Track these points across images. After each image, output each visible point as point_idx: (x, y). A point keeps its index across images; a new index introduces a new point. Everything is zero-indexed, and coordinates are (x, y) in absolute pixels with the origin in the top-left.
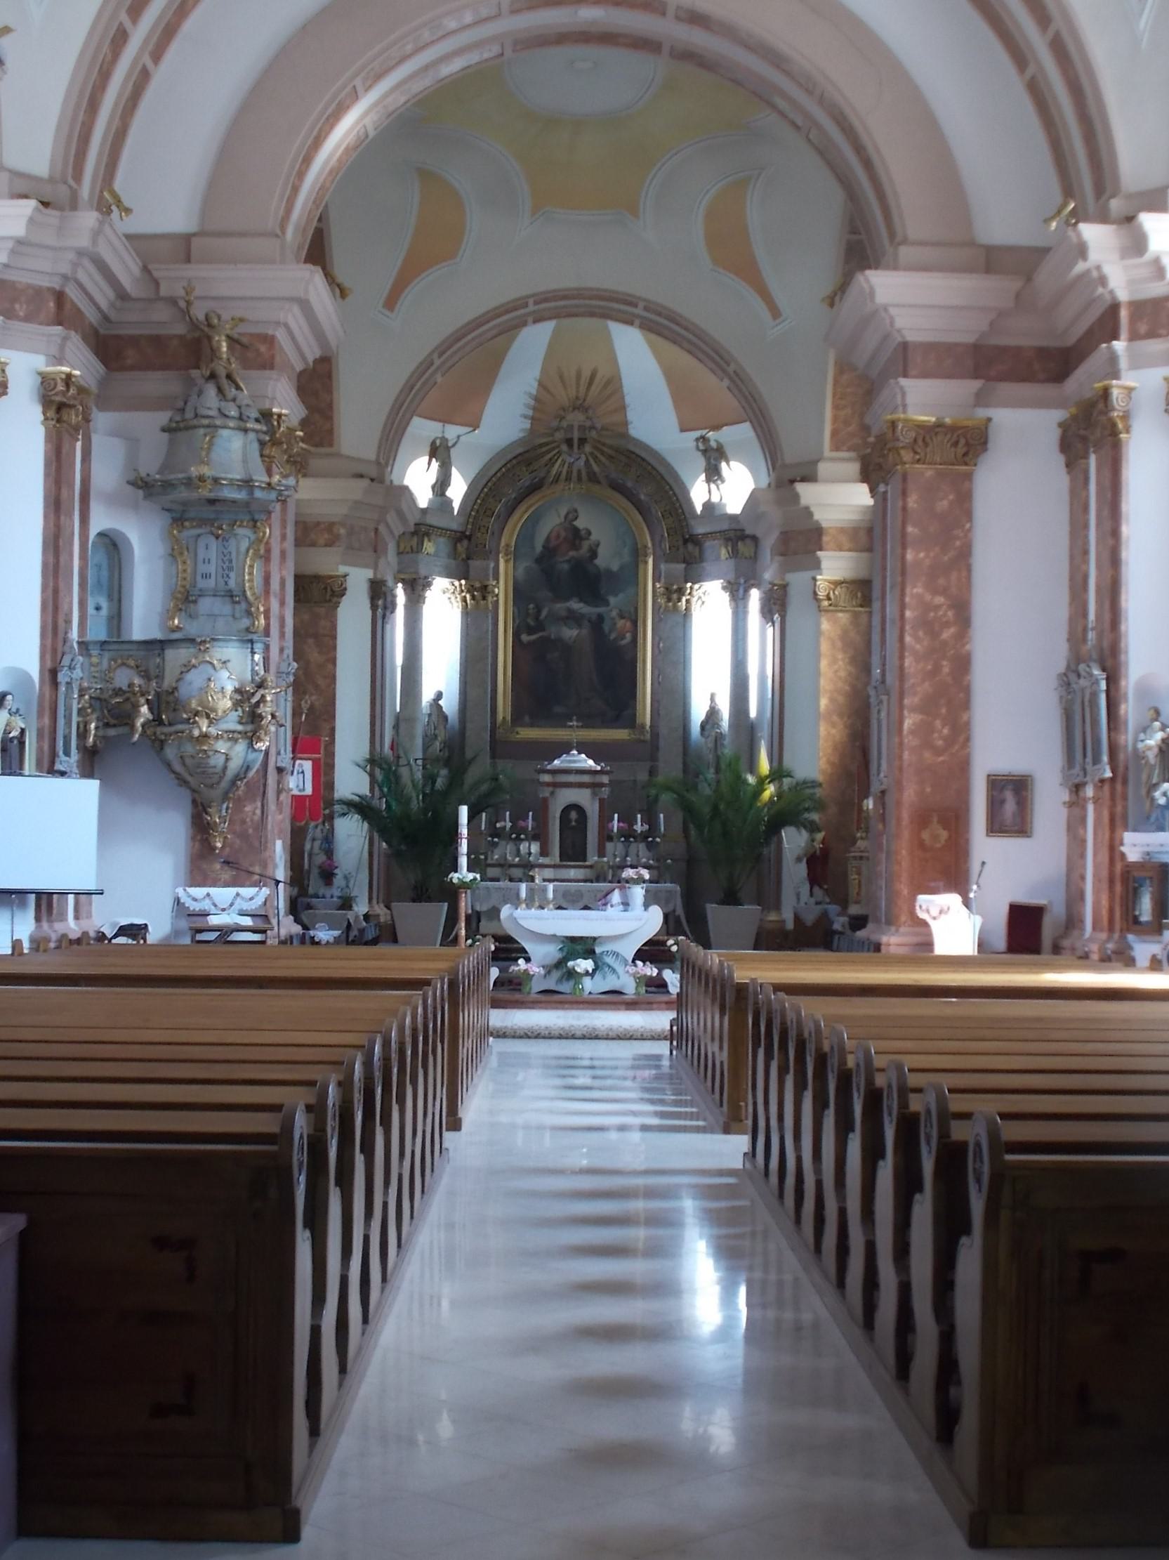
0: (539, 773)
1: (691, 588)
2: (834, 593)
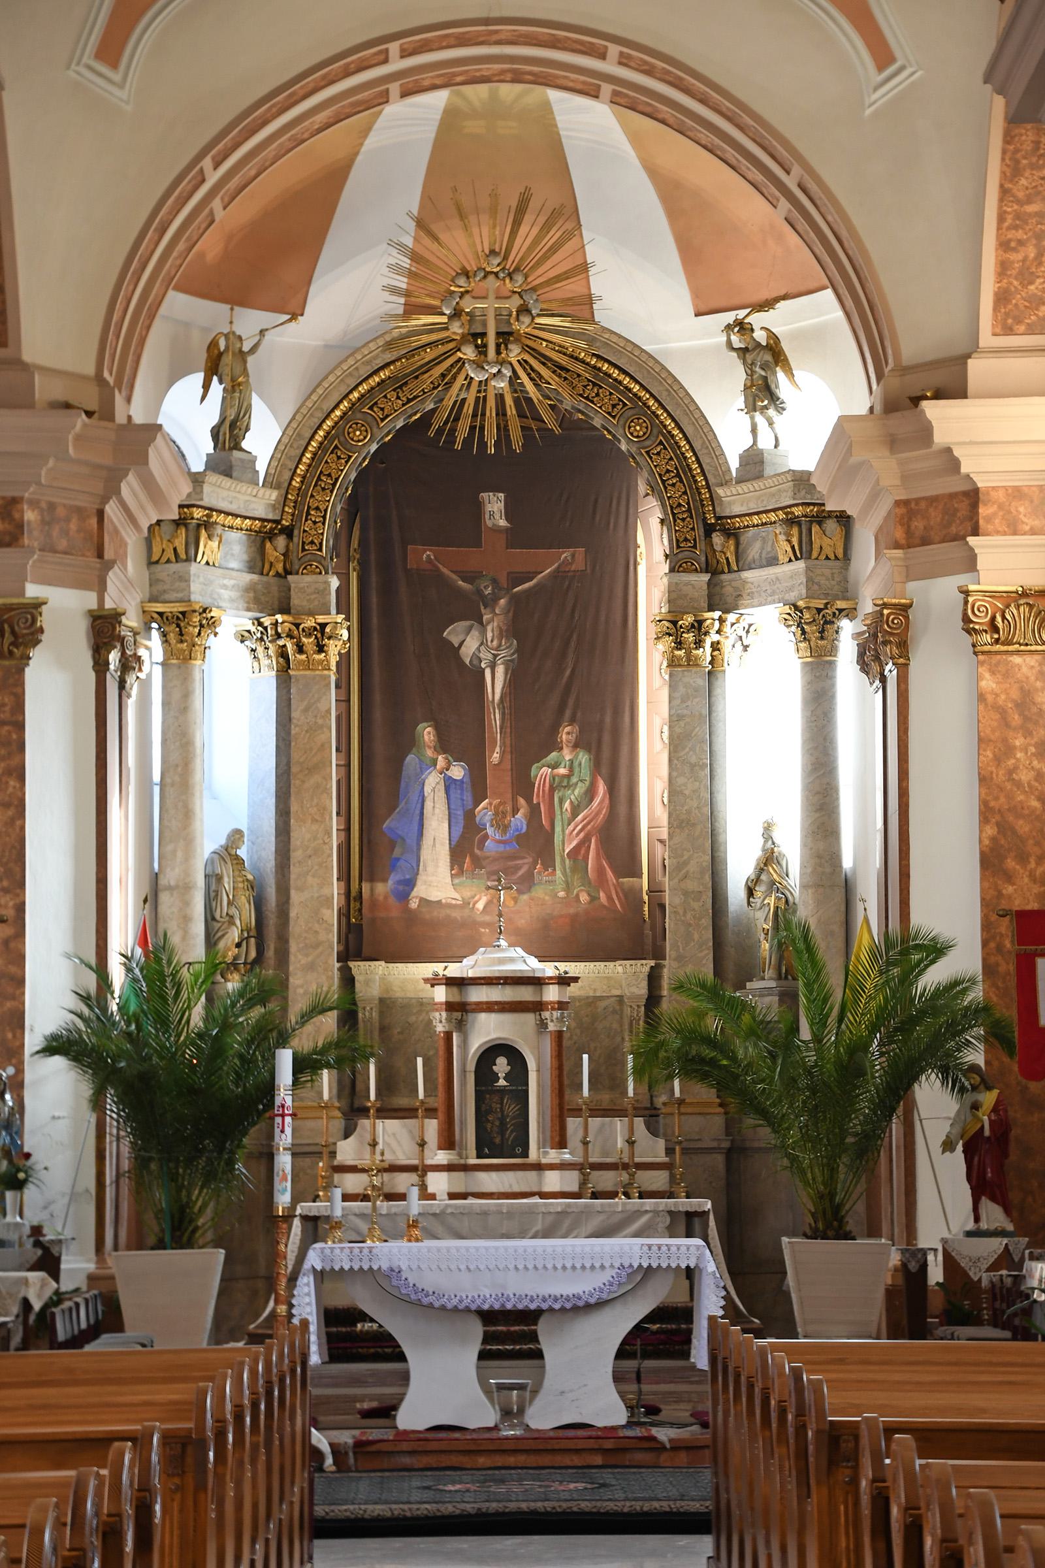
0: (433, 986)
1: (722, 620)
2: (1004, 618)
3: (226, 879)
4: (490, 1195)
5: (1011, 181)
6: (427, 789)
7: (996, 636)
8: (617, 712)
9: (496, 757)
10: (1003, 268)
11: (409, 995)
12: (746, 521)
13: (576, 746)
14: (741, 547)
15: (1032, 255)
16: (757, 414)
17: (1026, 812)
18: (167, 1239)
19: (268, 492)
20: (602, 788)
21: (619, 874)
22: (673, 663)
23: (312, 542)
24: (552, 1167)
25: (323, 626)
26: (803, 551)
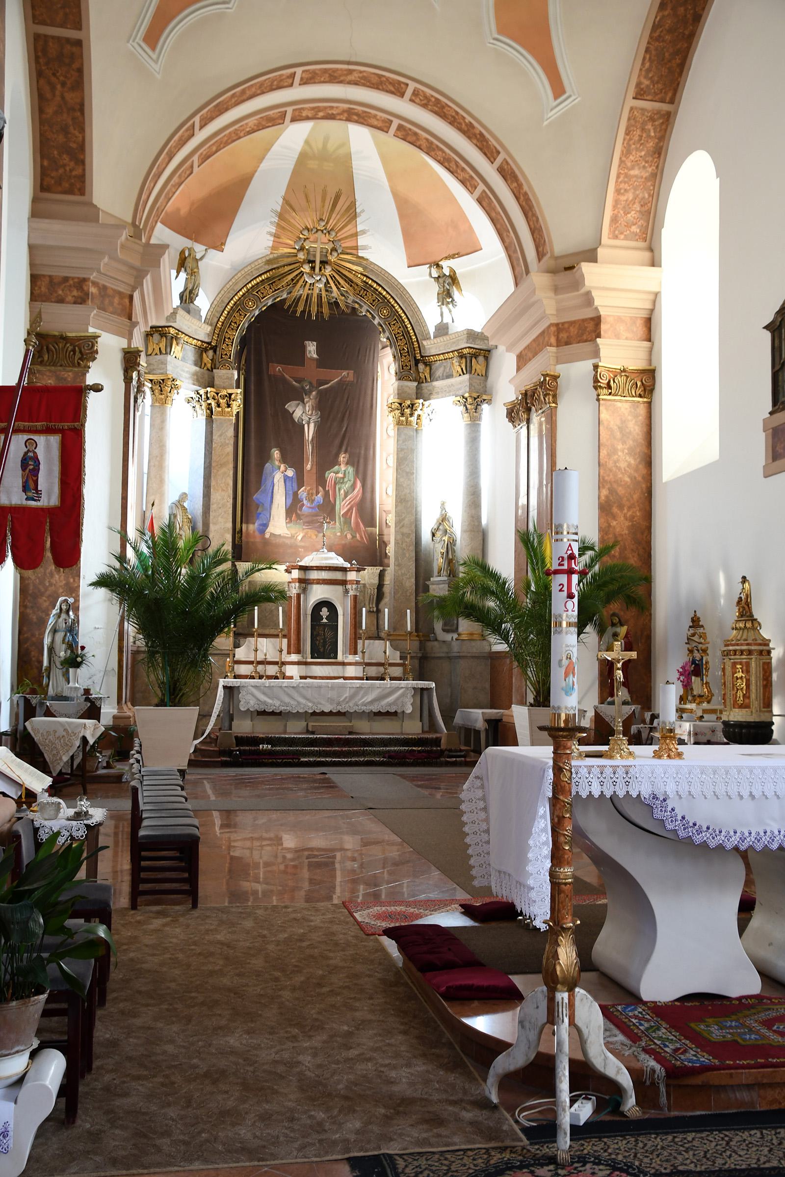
2: (614, 382)
3: (178, 516)
4: (315, 678)
5: (625, 156)
6: (276, 480)
7: (610, 391)
8: (367, 449)
9: (309, 467)
10: (616, 202)
11: (263, 580)
12: (437, 358)
13: (347, 464)
14: (432, 371)
15: (631, 198)
16: (444, 307)
17: (623, 483)
18: (167, 699)
19: (207, 326)
20: (359, 484)
21: (366, 526)
22: (399, 423)
23: (226, 354)
24: (350, 664)
25: (230, 395)
26: (469, 370)
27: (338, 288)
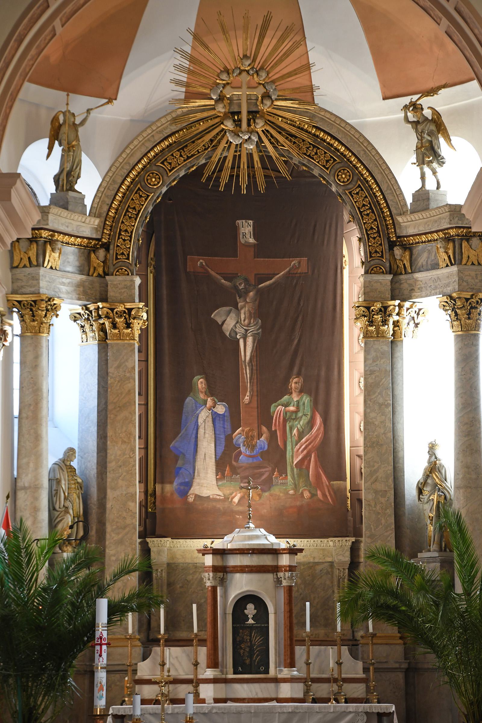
6: (200, 421)
8: (329, 369)
9: (247, 398)
13: (301, 391)
14: (414, 257)
19: (93, 219)
20: (319, 420)
21: (330, 478)
22: (367, 335)
24: (285, 680)
25: (130, 310)
27: (275, 147)
